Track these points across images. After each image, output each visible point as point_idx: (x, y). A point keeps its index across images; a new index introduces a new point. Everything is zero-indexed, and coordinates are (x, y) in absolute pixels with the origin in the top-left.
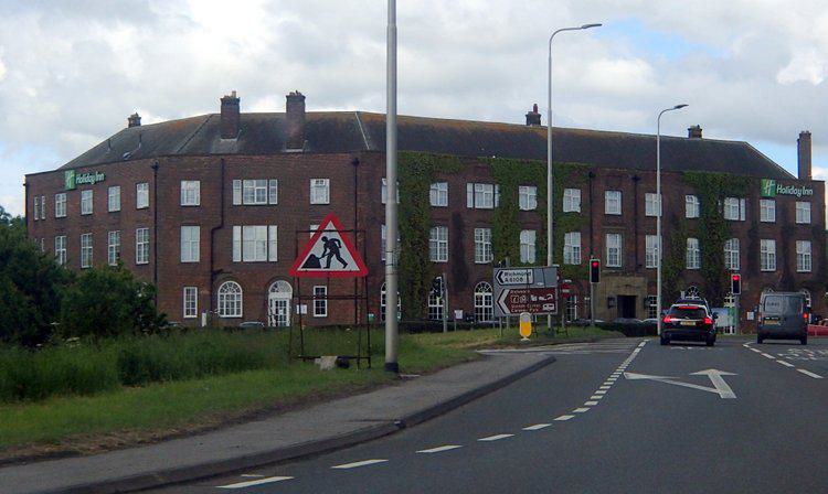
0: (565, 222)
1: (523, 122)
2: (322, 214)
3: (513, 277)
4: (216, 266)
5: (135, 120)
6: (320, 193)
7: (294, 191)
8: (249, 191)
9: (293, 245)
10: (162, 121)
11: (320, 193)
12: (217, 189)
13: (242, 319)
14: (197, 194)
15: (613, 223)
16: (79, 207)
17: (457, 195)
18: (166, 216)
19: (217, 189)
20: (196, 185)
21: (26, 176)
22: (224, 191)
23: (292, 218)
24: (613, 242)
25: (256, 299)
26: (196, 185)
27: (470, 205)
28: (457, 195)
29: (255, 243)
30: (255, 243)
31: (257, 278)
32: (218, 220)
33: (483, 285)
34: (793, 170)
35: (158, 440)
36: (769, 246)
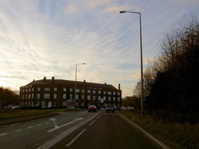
1: (104, 84)
2: (55, 92)
3: (69, 101)
4: (42, 99)
5: (34, 80)
6: (55, 89)
9: (52, 96)
11: (55, 89)
15: (94, 95)
16: (32, 90)
17: (107, 93)
18: (36, 92)
20: (40, 88)
21: (20, 87)
23: (52, 93)
24: (39, 95)
26: (40, 88)
28: (107, 93)
29: (47, 96)
30: (47, 96)
31: (47, 101)
35: (26, 121)
36: (114, 98)
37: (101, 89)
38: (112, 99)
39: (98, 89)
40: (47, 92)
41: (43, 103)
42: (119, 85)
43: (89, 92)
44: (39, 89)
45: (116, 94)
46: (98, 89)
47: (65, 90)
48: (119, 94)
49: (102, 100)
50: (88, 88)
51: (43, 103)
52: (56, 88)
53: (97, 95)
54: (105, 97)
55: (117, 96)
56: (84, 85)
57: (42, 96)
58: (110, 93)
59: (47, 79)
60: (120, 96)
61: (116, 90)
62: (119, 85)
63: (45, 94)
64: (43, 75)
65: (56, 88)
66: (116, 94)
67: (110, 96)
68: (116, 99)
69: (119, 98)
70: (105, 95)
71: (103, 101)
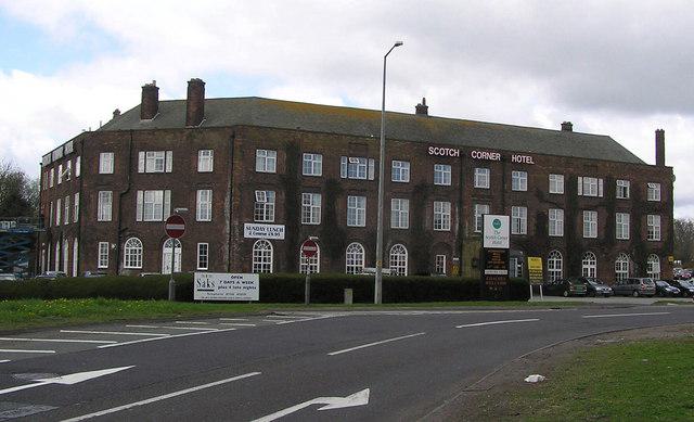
0: (396, 191)
1: (414, 112)
2: (205, 181)
4: (126, 222)
6: (205, 163)
7: (185, 160)
8: (149, 163)
10: (260, 420)
11: (205, 163)
12: (127, 162)
13: (142, 270)
14: (487, 181)
17: (571, 185)
19: (127, 162)
22: (132, 162)
23: (182, 184)
25: (153, 256)
27: (580, 194)
31: (154, 237)
32: (128, 183)
33: (359, 247)
34: (650, 160)
37: (528, 160)
38: (608, 226)
39: (506, 158)
40: (155, 181)
41: (133, 247)
42: (660, 135)
43: (444, 176)
44: (107, 164)
45: (638, 192)
46: (506, 158)
47: (267, 162)
48: (655, 193)
49: (497, 224)
50: (432, 151)
51: (133, 247)
52: (103, 171)
53: (462, 196)
54: (521, 214)
55: (640, 208)
56: (420, 138)
57: (125, 205)
58: (591, 187)
59: (162, 97)
60: (665, 207)
61: (639, 165)
62: (660, 135)
63: (140, 194)
64: (92, 42)
65: (103, 171)
66: (638, 192)
67: (591, 204)
68: (638, 227)
69: (655, 222)
70: (520, 198)
71: (504, 230)
